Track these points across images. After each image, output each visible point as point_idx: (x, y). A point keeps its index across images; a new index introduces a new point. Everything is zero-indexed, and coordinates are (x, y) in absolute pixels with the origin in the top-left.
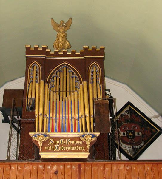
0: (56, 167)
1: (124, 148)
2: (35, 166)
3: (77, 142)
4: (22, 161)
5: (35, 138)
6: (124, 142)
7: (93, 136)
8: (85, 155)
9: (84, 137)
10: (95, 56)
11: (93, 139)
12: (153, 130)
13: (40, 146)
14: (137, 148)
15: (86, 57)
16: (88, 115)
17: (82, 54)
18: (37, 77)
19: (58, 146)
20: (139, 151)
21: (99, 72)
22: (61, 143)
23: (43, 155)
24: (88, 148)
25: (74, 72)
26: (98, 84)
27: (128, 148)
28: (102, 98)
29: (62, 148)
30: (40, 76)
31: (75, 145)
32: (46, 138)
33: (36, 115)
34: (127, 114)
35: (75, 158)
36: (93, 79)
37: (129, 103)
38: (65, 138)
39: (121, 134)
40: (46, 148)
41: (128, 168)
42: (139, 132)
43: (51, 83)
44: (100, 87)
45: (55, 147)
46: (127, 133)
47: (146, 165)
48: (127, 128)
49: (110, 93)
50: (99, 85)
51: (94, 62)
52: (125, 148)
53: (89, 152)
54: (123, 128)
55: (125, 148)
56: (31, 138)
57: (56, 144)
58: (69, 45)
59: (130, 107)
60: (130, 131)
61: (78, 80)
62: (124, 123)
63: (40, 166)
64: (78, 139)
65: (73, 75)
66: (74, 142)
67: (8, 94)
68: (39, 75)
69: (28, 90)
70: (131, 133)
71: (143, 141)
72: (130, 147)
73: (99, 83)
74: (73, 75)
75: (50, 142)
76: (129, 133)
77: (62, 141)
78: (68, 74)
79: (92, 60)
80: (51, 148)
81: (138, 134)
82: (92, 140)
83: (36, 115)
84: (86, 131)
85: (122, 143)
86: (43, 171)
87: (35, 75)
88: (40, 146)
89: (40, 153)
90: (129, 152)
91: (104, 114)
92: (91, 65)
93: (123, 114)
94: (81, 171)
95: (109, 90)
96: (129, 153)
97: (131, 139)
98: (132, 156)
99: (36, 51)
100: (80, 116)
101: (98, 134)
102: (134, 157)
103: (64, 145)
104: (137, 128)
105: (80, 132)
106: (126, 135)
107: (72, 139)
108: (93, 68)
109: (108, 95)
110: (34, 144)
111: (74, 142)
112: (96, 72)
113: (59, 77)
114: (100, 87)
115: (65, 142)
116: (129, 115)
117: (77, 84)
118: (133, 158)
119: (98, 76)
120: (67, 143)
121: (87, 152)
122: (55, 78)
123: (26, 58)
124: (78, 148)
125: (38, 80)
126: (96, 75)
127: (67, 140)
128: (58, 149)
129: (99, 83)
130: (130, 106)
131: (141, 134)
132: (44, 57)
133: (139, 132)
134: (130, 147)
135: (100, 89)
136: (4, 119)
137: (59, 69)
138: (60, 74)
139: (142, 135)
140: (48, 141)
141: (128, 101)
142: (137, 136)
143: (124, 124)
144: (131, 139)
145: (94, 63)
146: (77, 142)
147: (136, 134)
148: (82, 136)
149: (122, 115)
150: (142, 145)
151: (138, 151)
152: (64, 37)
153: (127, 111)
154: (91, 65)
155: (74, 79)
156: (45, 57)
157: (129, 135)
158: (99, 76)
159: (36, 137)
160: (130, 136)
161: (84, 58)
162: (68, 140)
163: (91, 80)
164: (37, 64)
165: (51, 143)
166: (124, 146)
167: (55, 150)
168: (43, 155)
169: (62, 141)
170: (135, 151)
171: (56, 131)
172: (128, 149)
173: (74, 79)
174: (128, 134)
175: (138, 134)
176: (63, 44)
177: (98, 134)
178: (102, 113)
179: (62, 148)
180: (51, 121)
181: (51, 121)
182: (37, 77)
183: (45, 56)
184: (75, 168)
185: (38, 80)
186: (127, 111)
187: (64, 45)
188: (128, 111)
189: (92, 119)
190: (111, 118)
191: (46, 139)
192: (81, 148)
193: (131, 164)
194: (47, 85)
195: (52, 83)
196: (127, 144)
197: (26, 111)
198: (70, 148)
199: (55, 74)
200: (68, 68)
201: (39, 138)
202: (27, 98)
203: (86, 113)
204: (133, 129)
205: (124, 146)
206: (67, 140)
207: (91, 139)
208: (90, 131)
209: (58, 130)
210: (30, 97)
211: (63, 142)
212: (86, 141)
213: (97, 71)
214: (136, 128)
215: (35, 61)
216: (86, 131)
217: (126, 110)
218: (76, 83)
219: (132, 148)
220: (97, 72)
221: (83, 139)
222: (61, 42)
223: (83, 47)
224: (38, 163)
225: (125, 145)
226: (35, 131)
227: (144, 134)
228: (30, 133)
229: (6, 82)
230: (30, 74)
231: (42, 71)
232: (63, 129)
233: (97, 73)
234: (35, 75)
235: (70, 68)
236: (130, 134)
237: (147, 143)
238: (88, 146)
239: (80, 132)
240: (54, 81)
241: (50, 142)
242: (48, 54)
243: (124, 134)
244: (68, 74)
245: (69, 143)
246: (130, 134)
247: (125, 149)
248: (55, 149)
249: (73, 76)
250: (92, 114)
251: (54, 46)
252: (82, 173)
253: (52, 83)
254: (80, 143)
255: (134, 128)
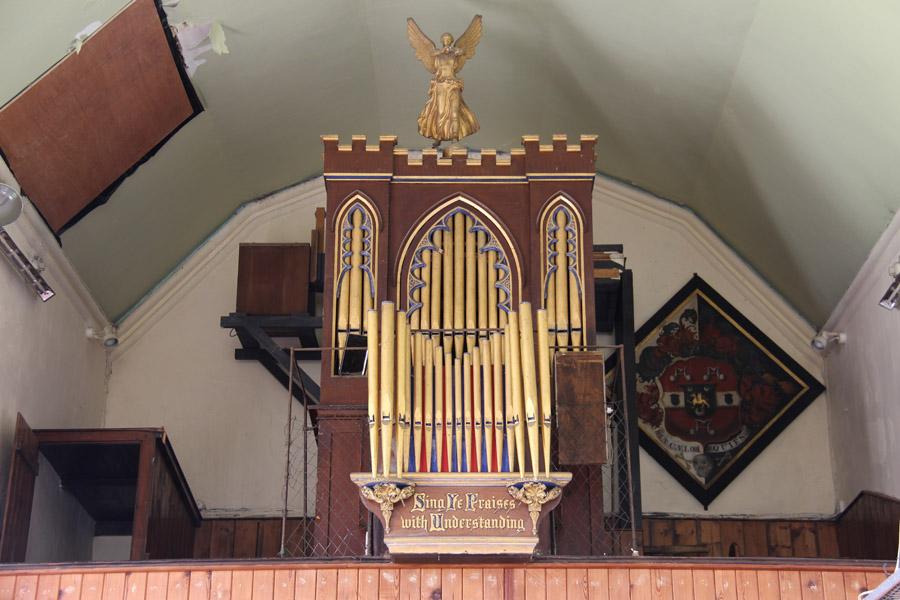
0: (436, 578)
1: (672, 453)
2: (371, 574)
3: (500, 503)
4: (332, 560)
5: (371, 492)
6: (674, 430)
7: (550, 487)
8: (527, 545)
9: (522, 490)
10: (553, 175)
11: (551, 496)
12: (784, 385)
13: (387, 517)
14: (721, 450)
15: (531, 177)
16: (536, 420)
17: (519, 165)
18: (366, 253)
19: (440, 517)
20: (729, 465)
21: (576, 231)
22: (452, 506)
23: (395, 545)
24: (534, 523)
25: (491, 232)
26: (572, 275)
27: (687, 452)
28: (585, 344)
29: (455, 522)
30: (374, 238)
31: (496, 513)
32: (403, 494)
33: (371, 418)
34: (687, 324)
35: (496, 555)
36: (555, 257)
37: (696, 283)
38: (461, 491)
39: (665, 401)
40: (405, 523)
41: (660, 583)
42: (731, 393)
43: (412, 272)
44: (579, 288)
45: (433, 518)
46: (688, 398)
47: (719, 573)
48: (688, 377)
49: (625, 259)
50: (577, 279)
51: (558, 195)
52: (679, 453)
53: (540, 534)
54: (672, 378)
55: (679, 453)
56: (355, 489)
57: (433, 510)
58: (455, 131)
59: (699, 297)
60: (698, 389)
61: (504, 262)
62: (675, 360)
63: (385, 574)
64: (501, 491)
65: (487, 242)
66: (492, 503)
67: (257, 262)
68: (372, 235)
69: (338, 300)
70: (700, 396)
71: (745, 427)
72: (697, 449)
73: (575, 275)
74: (487, 242)
75: (417, 502)
76: (694, 395)
77: (452, 499)
78: (471, 238)
79: (551, 189)
80: (420, 522)
81: (729, 399)
82: (547, 499)
83: (371, 418)
84: (528, 468)
85: (666, 434)
86: (397, 592)
87: (357, 246)
88: (387, 517)
89: (386, 540)
90: (692, 465)
91: (588, 398)
92: (549, 207)
93: (672, 325)
94: (513, 591)
95: (619, 249)
96: (693, 471)
97: (701, 417)
98: (702, 480)
99: (359, 157)
100: (509, 418)
101: (566, 477)
102: (709, 484)
103: (462, 513)
104: (725, 376)
105: (509, 471)
106: (682, 403)
107: (486, 492)
108: (555, 219)
109: (618, 266)
110: (363, 509)
111: (492, 503)
112: (567, 232)
113: (441, 251)
114: (579, 288)
115: (464, 502)
116: (694, 329)
117: (501, 277)
118: (706, 488)
119: (571, 247)
120: (470, 507)
121: (532, 536)
122: (426, 255)
123: (326, 182)
124: (503, 521)
125: (369, 265)
126: (567, 244)
127: (470, 496)
128: (440, 526)
129: (575, 275)
130: (698, 291)
131: (736, 400)
132: (387, 177)
133: (731, 393)
134: (697, 449)
135: (580, 295)
136: (240, 347)
137: (440, 223)
138: (442, 240)
139: (743, 403)
140: (409, 500)
141: (695, 275)
142: (723, 408)
143: (677, 362)
144: (701, 417)
145: (558, 199)
146: (500, 503)
147: (721, 401)
148: (514, 486)
149: (667, 329)
150: (740, 441)
151: (726, 462)
152: (456, 95)
153: (687, 314)
154: (549, 207)
155: (492, 255)
156: (391, 178)
157: (695, 401)
158: (574, 247)
159: (373, 490)
160: (698, 406)
161: (524, 180)
162: (473, 498)
163: (548, 263)
164: (365, 206)
165: (420, 505)
166: (674, 445)
167: (432, 529)
168: (395, 545)
169: (452, 499)
170: (715, 463)
171: (434, 470)
172: (689, 456)
173: (492, 255)
174: (692, 399)
175: (729, 399)
176: (451, 122)
177: (566, 477)
178: (582, 397)
179: (455, 522)
180: (418, 434)
181: (418, 434)
182: (366, 253)
183: (390, 175)
184: (495, 580)
185: (369, 265)
186: (687, 311)
187: (455, 124)
188: (693, 310)
189: (547, 432)
190: (610, 410)
191: (404, 496)
192: (513, 523)
193: (672, 568)
194: (402, 316)
195: (416, 272)
196: (687, 437)
197: (332, 375)
198: (478, 521)
199: (424, 242)
200: (471, 216)
201: (384, 494)
202: (333, 345)
203: (527, 411)
204: (708, 380)
205: (674, 445)
206: (470, 496)
207: (543, 495)
208: (542, 469)
209: (429, 467)
210: (342, 325)
211: (456, 503)
212: (529, 502)
213: (569, 227)
214: (722, 377)
215: (357, 193)
216: (528, 468)
217: (688, 307)
218: (498, 270)
219: (705, 450)
220: (571, 230)
221: (520, 495)
222: (443, 114)
223: (523, 139)
224: (379, 565)
225: (677, 441)
226: (369, 470)
227: (748, 398)
228: (354, 476)
229: (243, 204)
230: (342, 242)
231: (381, 231)
232: (433, 464)
233: (571, 235)
234: (357, 246)
235: (477, 219)
236: (699, 400)
237: (760, 435)
238: (535, 517)
239: (509, 471)
240: (424, 265)
241: (417, 502)
242: (399, 165)
243: (675, 399)
244: (471, 238)
245: (476, 506)
246: (699, 400)
247: (677, 456)
248: (432, 525)
249: (488, 245)
250: (547, 411)
251: (419, 129)
252: (516, 593)
253: (416, 272)
254: (508, 507)
255: (713, 376)
